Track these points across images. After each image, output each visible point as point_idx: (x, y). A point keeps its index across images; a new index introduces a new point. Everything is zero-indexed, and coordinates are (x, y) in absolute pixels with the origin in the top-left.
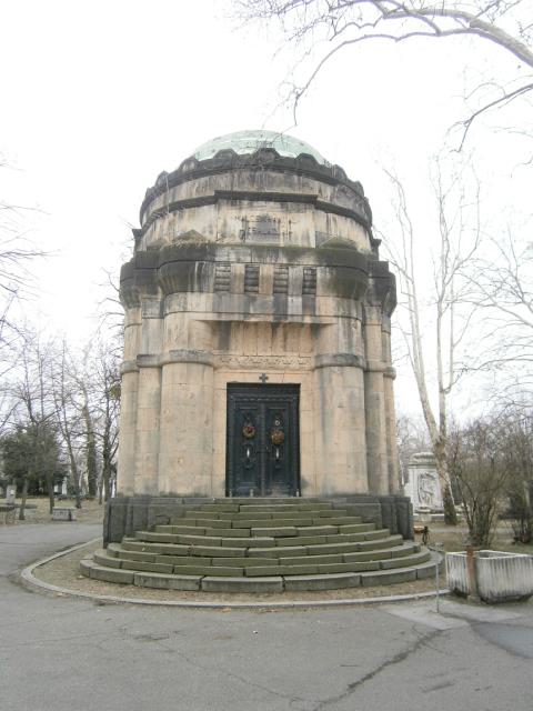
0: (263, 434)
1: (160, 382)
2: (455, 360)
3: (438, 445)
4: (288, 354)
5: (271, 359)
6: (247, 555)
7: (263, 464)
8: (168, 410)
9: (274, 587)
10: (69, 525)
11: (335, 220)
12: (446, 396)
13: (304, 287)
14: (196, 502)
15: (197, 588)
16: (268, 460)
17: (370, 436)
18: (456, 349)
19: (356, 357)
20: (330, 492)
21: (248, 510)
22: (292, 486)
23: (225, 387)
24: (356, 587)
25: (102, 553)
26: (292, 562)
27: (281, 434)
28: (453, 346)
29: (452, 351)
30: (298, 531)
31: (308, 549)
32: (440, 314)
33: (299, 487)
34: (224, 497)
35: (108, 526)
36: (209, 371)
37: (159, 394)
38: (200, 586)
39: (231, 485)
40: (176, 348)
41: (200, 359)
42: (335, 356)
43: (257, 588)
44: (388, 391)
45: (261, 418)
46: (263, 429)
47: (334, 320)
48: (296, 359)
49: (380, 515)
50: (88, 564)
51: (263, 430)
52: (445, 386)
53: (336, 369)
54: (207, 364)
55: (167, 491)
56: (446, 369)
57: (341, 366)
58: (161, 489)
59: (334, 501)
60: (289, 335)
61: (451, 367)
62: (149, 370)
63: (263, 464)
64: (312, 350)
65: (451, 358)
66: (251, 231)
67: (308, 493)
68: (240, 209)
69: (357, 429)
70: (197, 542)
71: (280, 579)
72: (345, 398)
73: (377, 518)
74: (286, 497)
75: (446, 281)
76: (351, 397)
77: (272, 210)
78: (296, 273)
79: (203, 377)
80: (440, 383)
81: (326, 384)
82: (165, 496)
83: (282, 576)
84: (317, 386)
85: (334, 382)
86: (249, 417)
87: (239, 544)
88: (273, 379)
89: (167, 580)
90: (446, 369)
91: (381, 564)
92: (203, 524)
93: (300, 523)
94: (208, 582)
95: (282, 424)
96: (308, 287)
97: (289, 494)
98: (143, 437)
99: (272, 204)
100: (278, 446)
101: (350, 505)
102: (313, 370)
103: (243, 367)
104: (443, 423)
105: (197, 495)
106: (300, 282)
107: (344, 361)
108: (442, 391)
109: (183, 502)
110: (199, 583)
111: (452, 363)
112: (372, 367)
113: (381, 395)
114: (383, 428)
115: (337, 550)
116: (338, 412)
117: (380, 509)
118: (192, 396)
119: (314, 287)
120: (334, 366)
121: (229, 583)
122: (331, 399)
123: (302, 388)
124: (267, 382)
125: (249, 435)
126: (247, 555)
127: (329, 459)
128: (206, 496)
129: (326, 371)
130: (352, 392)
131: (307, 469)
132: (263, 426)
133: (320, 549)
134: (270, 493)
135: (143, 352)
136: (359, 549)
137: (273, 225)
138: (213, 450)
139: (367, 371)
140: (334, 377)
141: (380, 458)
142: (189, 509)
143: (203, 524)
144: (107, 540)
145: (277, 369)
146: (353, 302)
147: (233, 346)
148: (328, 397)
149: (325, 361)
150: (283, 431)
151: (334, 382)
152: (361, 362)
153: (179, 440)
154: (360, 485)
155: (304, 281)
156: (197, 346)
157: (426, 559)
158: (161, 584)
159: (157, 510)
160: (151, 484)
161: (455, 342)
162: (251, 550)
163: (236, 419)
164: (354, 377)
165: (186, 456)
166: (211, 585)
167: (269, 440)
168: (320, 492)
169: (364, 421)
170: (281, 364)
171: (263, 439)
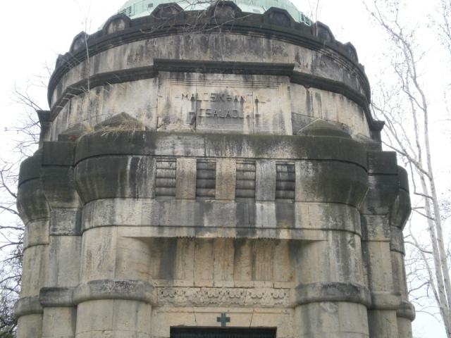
4: (257, 284)
5: (233, 292)
11: (318, 97)
13: (278, 189)
36: (145, 310)
41: (133, 293)
42: (325, 287)
47: (322, 235)
53: (327, 306)
54: (142, 300)
57: (334, 301)
62: (58, 312)
64: (291, 279)
66: (204, 114)
68: (189, 84)
77: (232, 86)
78: (266, 170)
85: (324, 324)
96: (284, 189)
99: (232, 77)
103: (195, 305)
106: (272, 183)
107: (338, 294)
112: (379, 302)
119: (293, 189)
120: (325, 301)
124: (228, 325)
129: (313, 308)
137: (233, 106)
139: (372, 309)
140: (325, 316)
146: (347, 210)
147: (179, 273)
149: (312, 294)
155: (278, 180)
170: (248, 300)
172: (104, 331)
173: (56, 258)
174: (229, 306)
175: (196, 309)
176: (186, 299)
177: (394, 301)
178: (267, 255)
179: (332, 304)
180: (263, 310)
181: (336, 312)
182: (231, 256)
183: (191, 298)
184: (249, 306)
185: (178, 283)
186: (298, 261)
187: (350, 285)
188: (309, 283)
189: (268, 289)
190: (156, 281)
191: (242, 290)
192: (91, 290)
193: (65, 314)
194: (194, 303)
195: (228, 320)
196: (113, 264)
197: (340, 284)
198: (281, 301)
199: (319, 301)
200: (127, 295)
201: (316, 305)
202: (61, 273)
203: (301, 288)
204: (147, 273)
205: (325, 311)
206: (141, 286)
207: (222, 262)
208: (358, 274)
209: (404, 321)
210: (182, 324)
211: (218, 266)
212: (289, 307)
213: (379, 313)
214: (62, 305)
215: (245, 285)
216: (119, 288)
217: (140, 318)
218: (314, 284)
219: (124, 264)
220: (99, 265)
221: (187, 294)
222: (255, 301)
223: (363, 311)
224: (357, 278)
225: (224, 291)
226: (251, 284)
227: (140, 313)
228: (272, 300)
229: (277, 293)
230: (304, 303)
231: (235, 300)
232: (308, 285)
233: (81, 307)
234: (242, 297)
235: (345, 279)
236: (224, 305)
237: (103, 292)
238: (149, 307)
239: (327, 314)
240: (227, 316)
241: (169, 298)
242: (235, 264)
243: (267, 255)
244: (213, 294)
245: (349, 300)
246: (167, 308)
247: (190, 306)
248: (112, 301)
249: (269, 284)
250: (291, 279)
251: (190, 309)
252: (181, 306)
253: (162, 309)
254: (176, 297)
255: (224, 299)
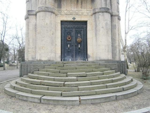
0: (74, 39)
1: (36, 21)
2: (130, 25)
3: (124, 48)
4: (83, 9)
5: (76, 12)
6: (64, 85)
7: (74, 50)
8: (38, 29)
9: (75, 103)
10: (4, 71)
12: (127, 35)
14: (49, 63)
15: (39, 101)
16: (76, 49)
17: (113, 40)
18: (130, 22)
19: (108, 9)
20: (98, 59)
21: (67, 66)
22: (84, 57)
23: (60, 22)
24: (114, 100)
25: (19, 80)
26: (84, 89)
27: (80, 39)
28: (129, 21)
29: (129, 22)
30: (87, 74)
31: (91, 83)
32: (126, 11)
33: (87, 57)
34: (60, 61)
35: (21, 71)
36: (53, 15)
37: (36, 25)
38: (41, 101)
39: (63, 57)
40: (40, 6)
41: (49, 10)
42: (101, 8)
43: (67, 103)
44: (119, 24)
45: (73, 34)
46: (74, 37)
48: (86, 11)
49: (117, 67)
50: (14, 85)
51: (74, 38)
52: (127, 32)
53: (101, 13)
54: (52, 12)
55: (39, 59)
56: (127, 27)
57: (103, 12)
58: (37, 58)
59: (100, 62)
60: (83, 3)
61: (128, 27)
62: (32, 16)
63: (74, 50)
64: (92, 8)
65: (129, 24)
67: (90, 59)
69: (108, 36)
70: (44, 79)
71: (77, 98)
72: (104, 25)
73: (116, 68)
74: (82, 61)
75: (128, 2)
76: (107, 24)
79: (51, 17)
80: (125, 31)
81: (97, 19)
82: (38, 61)
83: (79, 96)
84: (94, 21)
85: (100, 18)
86: (69, 33)
87: (61, 80)
88: (78, 19)
89: (27, 97)
90: (127, 27)
91: (123, 88)
92: (49, 71)
93: (88, 71)
94: (44, 99)
95: (81, 36)
97: (84, 60)
98: (31, 41)
100: (79, 43)
101: (106, 63)
102: (92, 15)
103: (66, 15)
104: (126, 42)
105: (49, 60)
107: (104, 10)
108: (126, 33)
109: (44, 63)
110: (40, 99)
111: (129, 26)
112: (114, 14)
113: (117, 24)
114: (117, 36)
115: (103, 83)
116: (101, 29)
117: (117, 65)
118: (47, 24)
120: (100, 12)
121: (54, 100)
122: (99, 25)
123: (88, 22)
124: (75, 20)
125: (69, 40)
126: (64, 85)
127: (98, 47)
128: (53, 61)
129: (97, 15)
130: (107, 22)
131: (89, 52)
132: (74, 36)
133: (97, 82)
134: (77, 60)
135: (30, 9)
136: (113, 81)
138: (56, 45)
139: (112, 16)
140: (100, 16)
141: (116, 47)
142: (46, 66)
143: (49, 71)
144: (21, 76)
145: (79, 15)
147: (63, 7)
148: (98, 24)
149: (97, 11)
150: (81, 38)
151: (100, 19)
152: (110, 11)
153: (42, 40)
154: (109, 56)
156: (49, 5)
157: (135, 86)
158: (25, 99)
159: (34, 66)
160: (34, 57)
161: (129, 20)
162: (66, 83)
163: (64, 34)
164: (107, 16)
165: (48, 48)
166: (45, 101)
167: (76, 41)
168: (94, 59)
169: (111, 32)
170: (80, 13)
171: (74, 41)
172: (42, 20)
173: (31, 3)
174: (75, 15)
175: (67, 16)
176: (64, 13)
177: (117, 13)
178: (85, 2)
179: (102, 13)
180: (84, 16)
181: (103, 15)
182: (76, 2)
183: (65, 13)
184: (81, 15)
185: (62, 9)
186: (93, 3)
187: (107, 8)
188: (96, 8)
189: (85, 11)
190: (57, 9)
191: (78, 11)
192: (39, 9)
193: (34, 17)
194: (66, 14)
195: (75, 19)
196: (44, 3)
197: (105, 8)
198: (89, 14)
199: (99, 12)
200: (48, 10)
201: (98, 13)
202: (33, 7)
203: (94, 9)
204: (54, 6)
205: (100, 15)
206: (52, 8)
207: (74, 4)
208: (109, 6)
209: (119, 20)
210: (63, 20)
211: (73, 5)
212: (91, 15)
213: (113, 17)
214: (33, 15)
215: (80, 10)
216: (46, 8)
217: (52, 17)
218: (98, 8)
219: (47, 3)
220: (41, 3)
221: (64, 12)
222: (82, 14)
223: (110, 15)
224: (109, 7)
225: (74, 11)
226: (81, 9)
227: (52, 16)
228: (86, 14)
229: (88, 12)
230: (95, 13)
231: (77, 14)
232: (96, 9)
233: (38, 14)
234: (79, 13)
235: (106, 7)
236: (74, 15)
237: (42, 9)
238: (55, 15)
239: (100, 16)
240: (75, 18)
241: (60, 13)
242: (77, 4)
243: (85, 2)
244: (71, 12)
245: (106, 12)
246: (59, 16)
247: (65, 15)
248: (44, 12)
249: (86, 10)
250: (92, 8)
251: (65, 16)
252: (63, 15)
253: (58, 16)
254: (62, 13)
255: (74, 13)
